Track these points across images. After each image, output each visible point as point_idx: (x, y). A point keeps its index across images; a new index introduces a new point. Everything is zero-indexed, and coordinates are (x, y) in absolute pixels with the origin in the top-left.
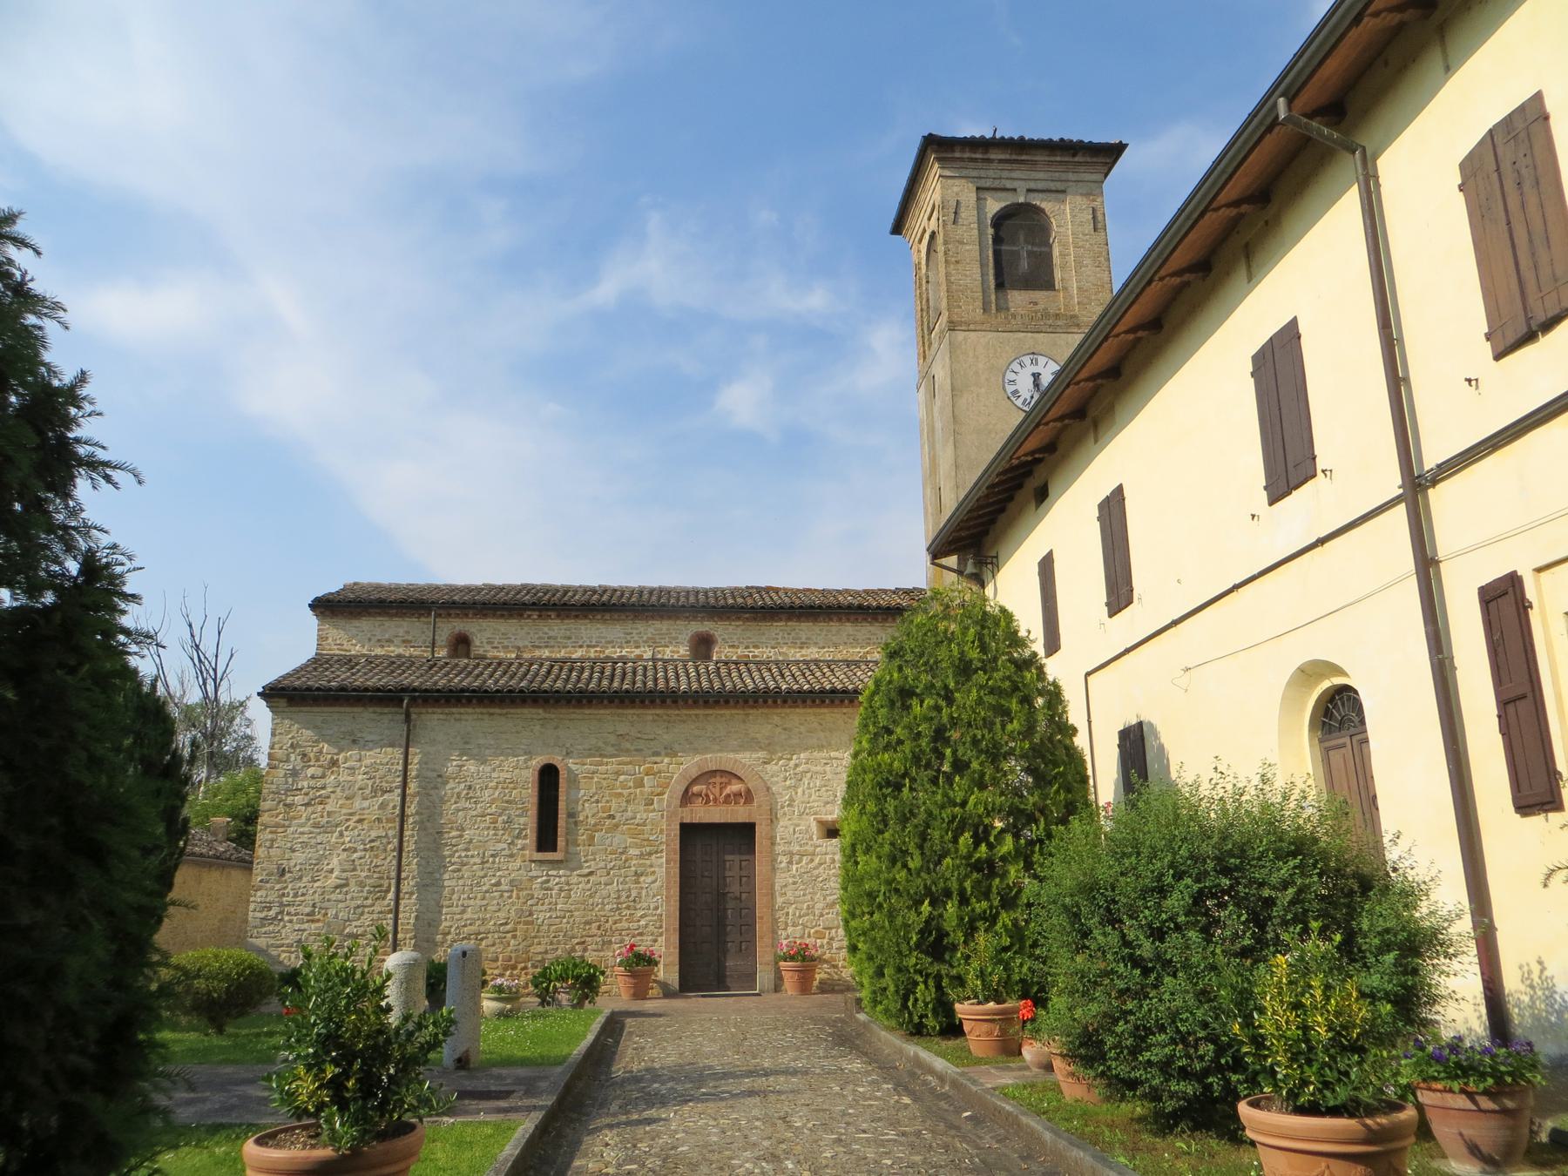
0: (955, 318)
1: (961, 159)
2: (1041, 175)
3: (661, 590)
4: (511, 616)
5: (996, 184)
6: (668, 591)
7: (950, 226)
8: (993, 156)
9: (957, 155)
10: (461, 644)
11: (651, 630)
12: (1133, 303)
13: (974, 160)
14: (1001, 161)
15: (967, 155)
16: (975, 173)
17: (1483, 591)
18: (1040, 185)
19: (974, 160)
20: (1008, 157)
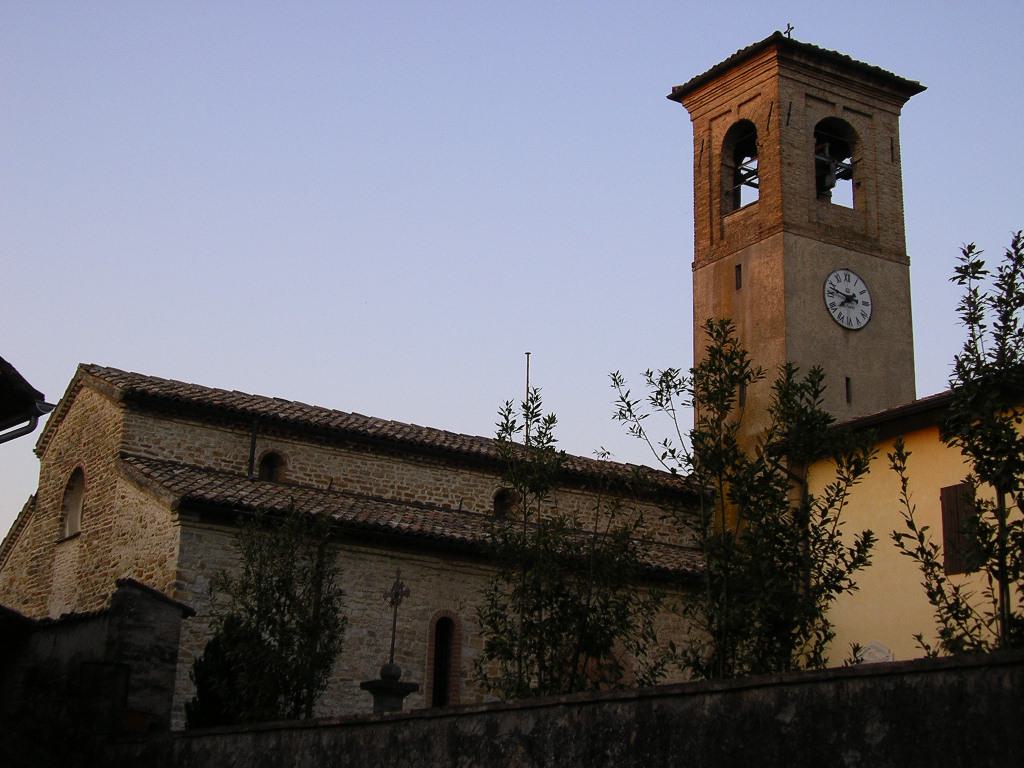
0: (787, 220)
1: (796, 63)
2: (853, 96)
3: (430, 430)
4: (328, 443)
5: (820, 95)
6: (420, 430)
7: (784, 128)
8: (823, 68)
9: (795, 58)
10: (271, 466)
11: (459, 479)
12: (750, 100)
13: (806, 66)
14: (828, 74)
15: (803, 61)
16: (804, 79)
17: (82, 366)
18: (854, 106)
19: (806, 66)
20: (834, 72)
